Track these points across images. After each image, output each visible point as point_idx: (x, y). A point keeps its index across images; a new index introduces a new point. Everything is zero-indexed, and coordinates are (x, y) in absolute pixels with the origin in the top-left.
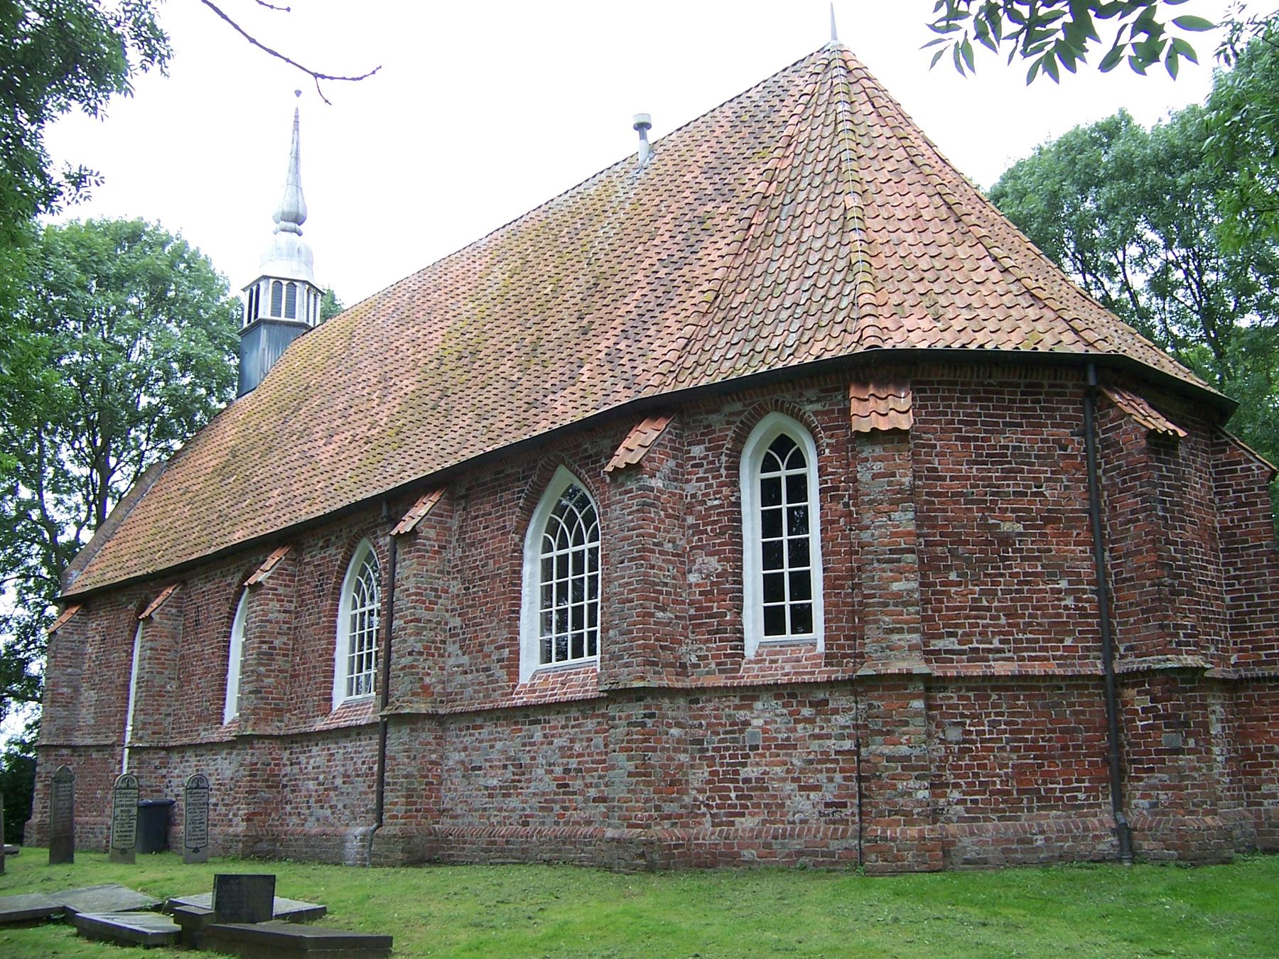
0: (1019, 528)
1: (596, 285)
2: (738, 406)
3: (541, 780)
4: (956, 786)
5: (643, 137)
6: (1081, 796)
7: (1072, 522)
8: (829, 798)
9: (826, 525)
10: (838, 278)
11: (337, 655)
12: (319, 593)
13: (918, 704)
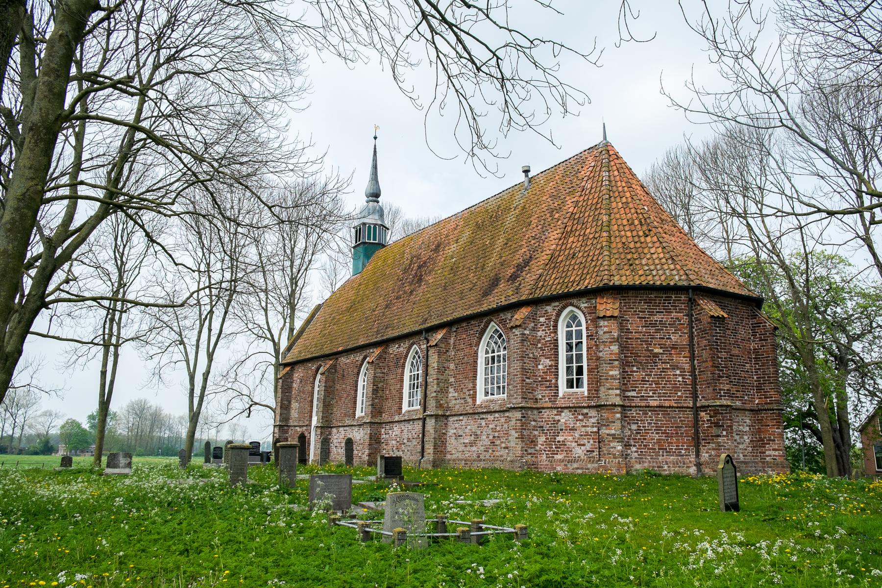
0: (661, 351)
1: (506, 244)
2: (557, 304)
3: (485, 440)
4: (635, 446)
5: (527, 176)
6: (683, 452)
7: (682, 349)
8: (588, 449)
9: (588, 348)
10: (597, 252)
11: (404, 391)
12: (397, 365)
13: (618, 416)
